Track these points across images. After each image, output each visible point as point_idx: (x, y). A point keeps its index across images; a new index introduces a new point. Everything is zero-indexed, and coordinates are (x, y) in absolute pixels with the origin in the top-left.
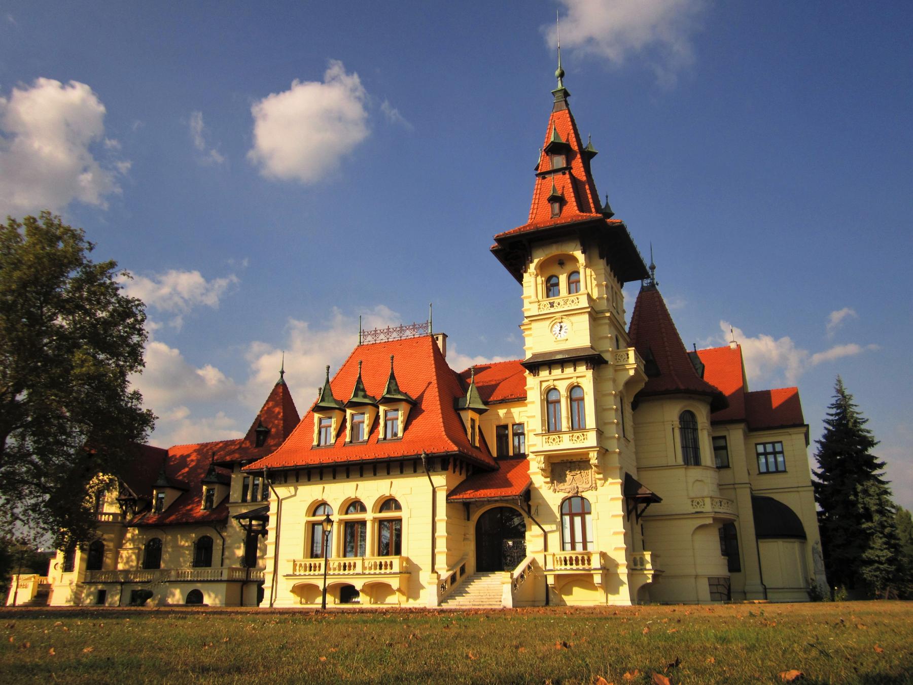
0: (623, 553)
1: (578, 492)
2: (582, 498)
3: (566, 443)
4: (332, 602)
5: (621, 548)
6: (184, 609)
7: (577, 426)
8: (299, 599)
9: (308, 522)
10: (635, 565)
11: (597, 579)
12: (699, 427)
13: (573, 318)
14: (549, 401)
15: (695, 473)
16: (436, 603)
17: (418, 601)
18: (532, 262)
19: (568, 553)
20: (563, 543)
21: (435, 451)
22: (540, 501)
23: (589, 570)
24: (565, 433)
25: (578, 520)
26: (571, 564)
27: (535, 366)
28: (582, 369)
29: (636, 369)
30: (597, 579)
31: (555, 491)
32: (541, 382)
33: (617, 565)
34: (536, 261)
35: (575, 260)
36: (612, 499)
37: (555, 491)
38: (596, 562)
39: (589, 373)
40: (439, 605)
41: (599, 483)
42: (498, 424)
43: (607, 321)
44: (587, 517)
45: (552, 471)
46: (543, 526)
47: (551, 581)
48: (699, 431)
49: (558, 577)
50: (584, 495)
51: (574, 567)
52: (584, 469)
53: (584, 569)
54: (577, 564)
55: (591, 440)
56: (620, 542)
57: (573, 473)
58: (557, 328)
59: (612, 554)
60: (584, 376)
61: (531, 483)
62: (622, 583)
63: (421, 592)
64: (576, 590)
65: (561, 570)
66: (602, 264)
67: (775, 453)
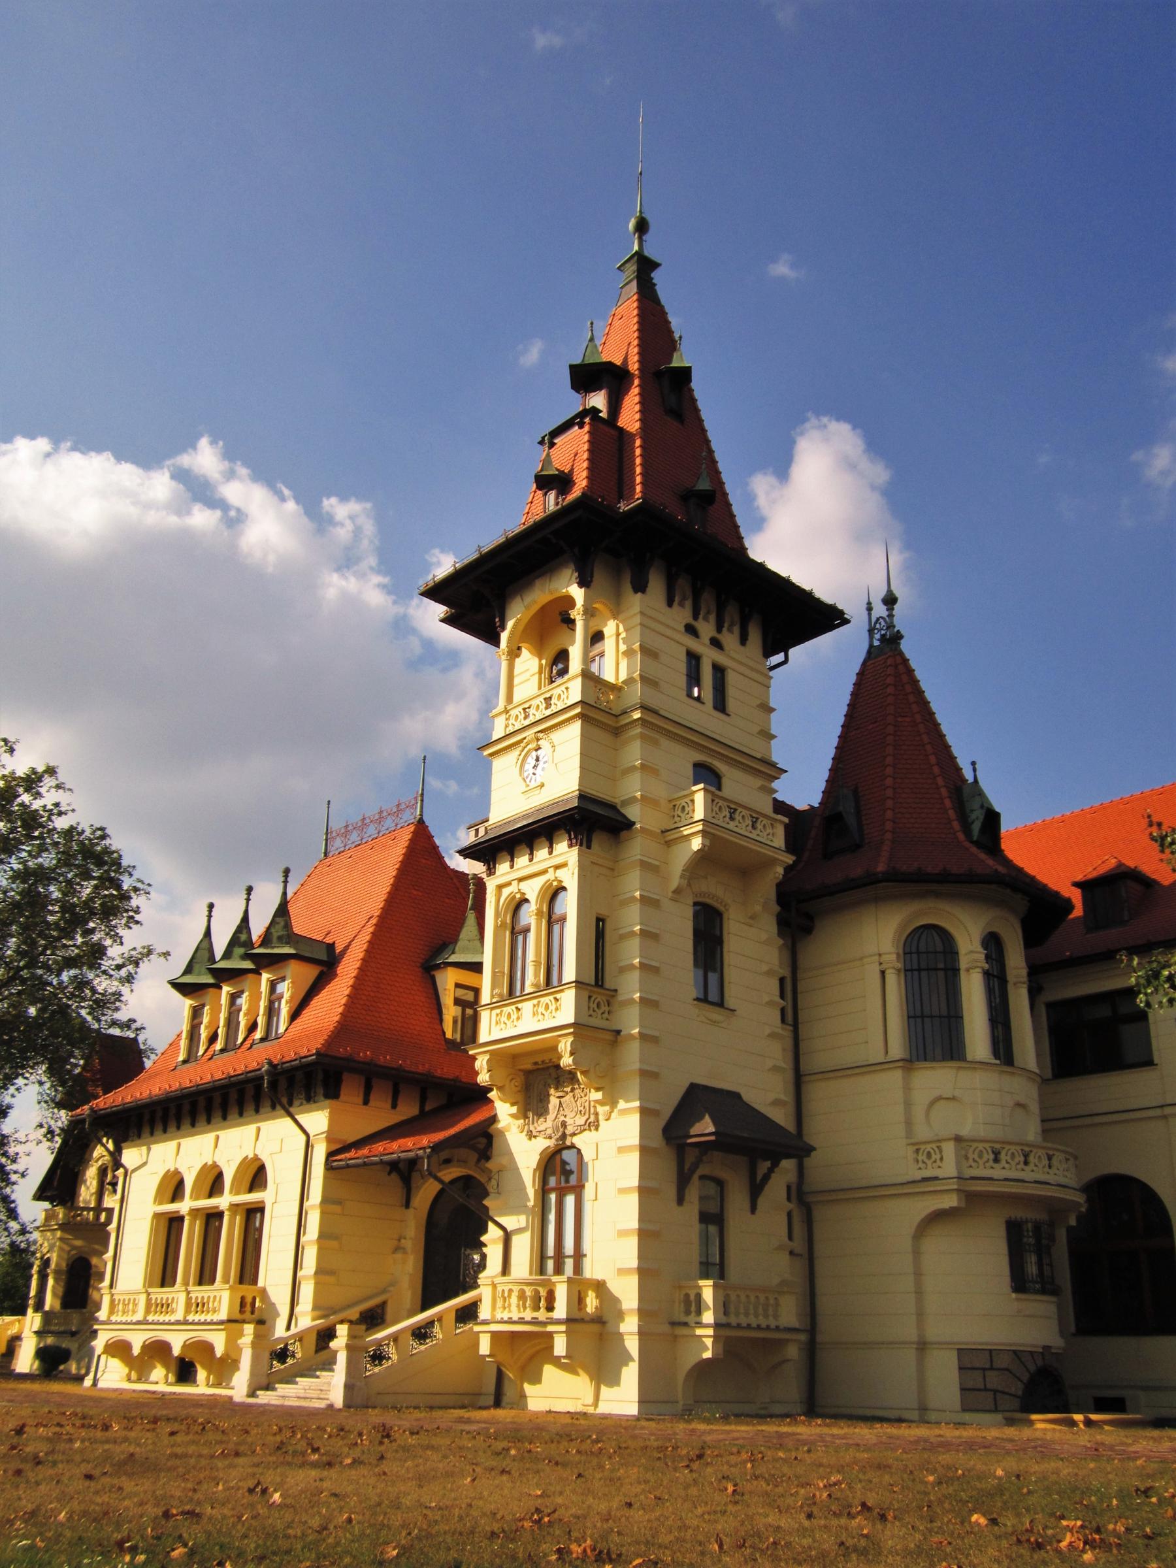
0: (634, 1280)
4: (160, 1380)
6: (36, 1387)
8: (126, 1370)
9: (157, 1216)
10: (666, 1317)
12: (963, 963)
15: (936, 1078)
22: (505, 1161)
25: (570, 1200)
31: (531, 1136)
41: (602, 1110)
43: (638, 730)
48: (963, 974)
58: (531, 761)
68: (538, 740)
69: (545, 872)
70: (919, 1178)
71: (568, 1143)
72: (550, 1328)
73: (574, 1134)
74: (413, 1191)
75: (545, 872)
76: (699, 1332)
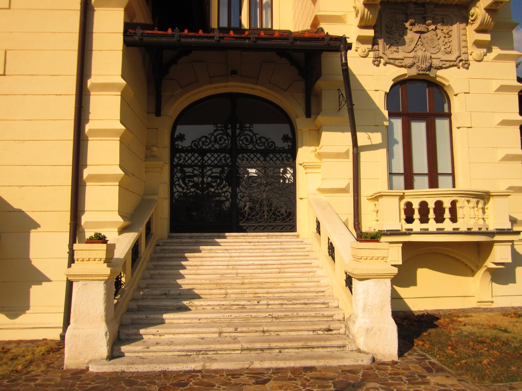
16: (104, 351)
17: (23, 319)
31: (377, 62)
37: (377, 62)
40: (114, 354)
44: (441, 124)
52: (443, 23)
63: (35, 291)
73: (441, 68)
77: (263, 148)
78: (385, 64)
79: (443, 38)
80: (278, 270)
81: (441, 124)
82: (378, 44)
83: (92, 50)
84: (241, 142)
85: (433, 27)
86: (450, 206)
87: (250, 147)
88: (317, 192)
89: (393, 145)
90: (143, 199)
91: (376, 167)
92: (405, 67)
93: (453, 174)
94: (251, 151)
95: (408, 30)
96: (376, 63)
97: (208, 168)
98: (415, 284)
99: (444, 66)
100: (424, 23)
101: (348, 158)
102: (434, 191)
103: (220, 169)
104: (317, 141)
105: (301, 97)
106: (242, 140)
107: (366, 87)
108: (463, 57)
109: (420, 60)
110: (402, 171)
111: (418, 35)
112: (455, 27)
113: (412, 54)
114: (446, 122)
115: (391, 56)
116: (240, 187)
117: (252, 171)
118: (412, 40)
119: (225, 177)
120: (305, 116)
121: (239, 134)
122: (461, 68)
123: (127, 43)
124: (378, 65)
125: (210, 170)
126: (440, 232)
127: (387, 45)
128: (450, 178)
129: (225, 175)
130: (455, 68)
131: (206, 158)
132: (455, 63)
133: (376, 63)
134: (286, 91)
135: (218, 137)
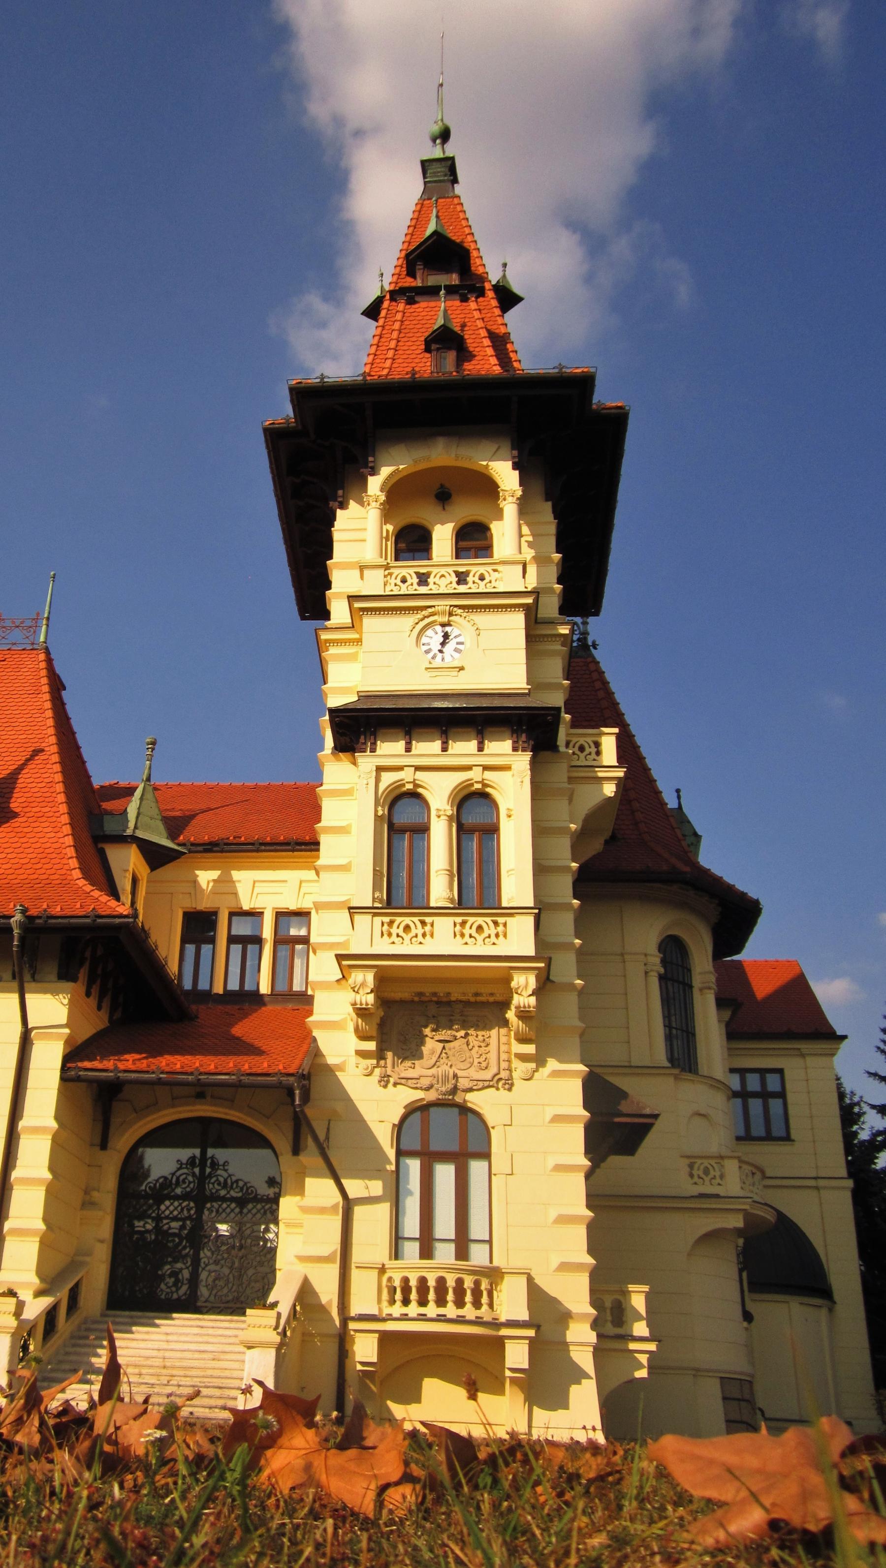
0: (583, 1281)
1: (454, 1090)
2: (465, 1110)
3: (443, 939)
5: (577, 1267)
7: (477, 891)
10: (611, 1318)
11: (517, 1355)
12: (697, 981)
13: (481, 619)
14: (400, 819)
18: (374, 472)
19: (412, 1266)
20: (397, 1239)
21: (57, 910)
22: (339, 1107)
23: (496, 1324)
24: (441, 911)
25: (445, 1174)
26: (423, 1303)
27: (358, 727)
28: (500, 748)
29: (620, 782)
30: (517, 1355)
31: (384, 1081)
32: (380, 769)
33: (565, 1317)
34: (386, 471)
35: (488, 489)
36: (557, 1119)
37: (384, 1081)
38: (511, 1303)
39: (522, 761)
42: (190, 904)
44: (477, 1168)
45: (383, 1026)
46: (345, 1182)
47: (365, 1349)
48: (696, 992)
49: (386, 1340)
50: (475, 1100)
51: (432, 1310)
52: (477, 1027)
53: (478, 1322)
54: (441, 1301)
55: (519, 938)
56: (575, 1246)
57: (445, 1034)
58: (434, 637)
59: (551, 1285)
60: (508, 773)
61: (317, 1053)
62: (579, 1375)
64: (432, 1387)
65: (404, 1317)
66: (546, 512)
67: (765, 1095)
68: (451, 614)
69: (468, 768)
70: (695, 1194)
71: (458, 1099)
72: (504, 1332)
73: (471, 1090)
74: (112, 1130)
75: (468, 768)
76: (633, 1346)
77: (240, 1195)
78: (395, 1084)
79: (476, 1048)
80: (210, 1356)
81: (477, 1168)
82: (385, 1059)
83: (26, 1088)
84: (211, 1186)
85: (462, 1033)
86: (472, 1286)
87: (223, 1193)
88: (296, 1261)
89: (406, 1197)
90: (73, 1261)
91: (372, 1226)
92: (421, 1089)
93: (490, 1242)
94: (223, 1199)
95: (427, 1039)
96: (383, 1083)
97: (165, 1221)
98: (417, 1399)
99: (475, 1088)
100: (451, 1028)
101: (337, 1214)
102: (426, 1263)
103: (181, 1223)
104: (300, 1190)
105: (288, 1126)
106: (213, 1184)
107: (367, 1117)
108: (504, 1074)
109: (440, 1080)
110: (453, 1237)
111: (441, 1045)
112: (494, 1032)
113: (433, 1071)
114: (484, 1164)
115: (403, 1075)
116: (206, 1250)
117: (223, 1228)
118: (433, 1052)
119: (187, 1234)
120: (291, 1153)
121: (210, 1173)
122: (502, 1089)
123: (64, 1079)
124: (385, 1086)
125: (167, 1223)
126: (422, 1318)
127: (399, 1059)
128: (487, 1246)
129: (186, 1232)
130: (493, 1089)
131: (163, 1207)
132: (491, 1083)
133: (383, 1083)
134: (268, 1118)
135: (181, 1178)
